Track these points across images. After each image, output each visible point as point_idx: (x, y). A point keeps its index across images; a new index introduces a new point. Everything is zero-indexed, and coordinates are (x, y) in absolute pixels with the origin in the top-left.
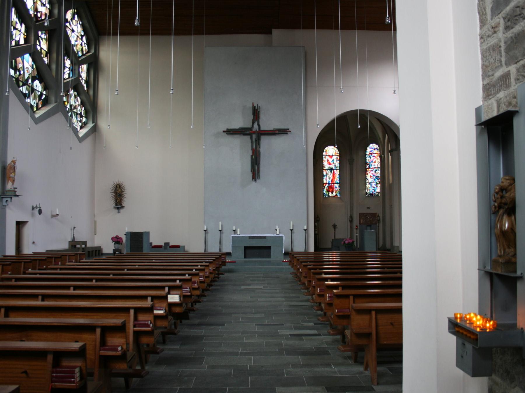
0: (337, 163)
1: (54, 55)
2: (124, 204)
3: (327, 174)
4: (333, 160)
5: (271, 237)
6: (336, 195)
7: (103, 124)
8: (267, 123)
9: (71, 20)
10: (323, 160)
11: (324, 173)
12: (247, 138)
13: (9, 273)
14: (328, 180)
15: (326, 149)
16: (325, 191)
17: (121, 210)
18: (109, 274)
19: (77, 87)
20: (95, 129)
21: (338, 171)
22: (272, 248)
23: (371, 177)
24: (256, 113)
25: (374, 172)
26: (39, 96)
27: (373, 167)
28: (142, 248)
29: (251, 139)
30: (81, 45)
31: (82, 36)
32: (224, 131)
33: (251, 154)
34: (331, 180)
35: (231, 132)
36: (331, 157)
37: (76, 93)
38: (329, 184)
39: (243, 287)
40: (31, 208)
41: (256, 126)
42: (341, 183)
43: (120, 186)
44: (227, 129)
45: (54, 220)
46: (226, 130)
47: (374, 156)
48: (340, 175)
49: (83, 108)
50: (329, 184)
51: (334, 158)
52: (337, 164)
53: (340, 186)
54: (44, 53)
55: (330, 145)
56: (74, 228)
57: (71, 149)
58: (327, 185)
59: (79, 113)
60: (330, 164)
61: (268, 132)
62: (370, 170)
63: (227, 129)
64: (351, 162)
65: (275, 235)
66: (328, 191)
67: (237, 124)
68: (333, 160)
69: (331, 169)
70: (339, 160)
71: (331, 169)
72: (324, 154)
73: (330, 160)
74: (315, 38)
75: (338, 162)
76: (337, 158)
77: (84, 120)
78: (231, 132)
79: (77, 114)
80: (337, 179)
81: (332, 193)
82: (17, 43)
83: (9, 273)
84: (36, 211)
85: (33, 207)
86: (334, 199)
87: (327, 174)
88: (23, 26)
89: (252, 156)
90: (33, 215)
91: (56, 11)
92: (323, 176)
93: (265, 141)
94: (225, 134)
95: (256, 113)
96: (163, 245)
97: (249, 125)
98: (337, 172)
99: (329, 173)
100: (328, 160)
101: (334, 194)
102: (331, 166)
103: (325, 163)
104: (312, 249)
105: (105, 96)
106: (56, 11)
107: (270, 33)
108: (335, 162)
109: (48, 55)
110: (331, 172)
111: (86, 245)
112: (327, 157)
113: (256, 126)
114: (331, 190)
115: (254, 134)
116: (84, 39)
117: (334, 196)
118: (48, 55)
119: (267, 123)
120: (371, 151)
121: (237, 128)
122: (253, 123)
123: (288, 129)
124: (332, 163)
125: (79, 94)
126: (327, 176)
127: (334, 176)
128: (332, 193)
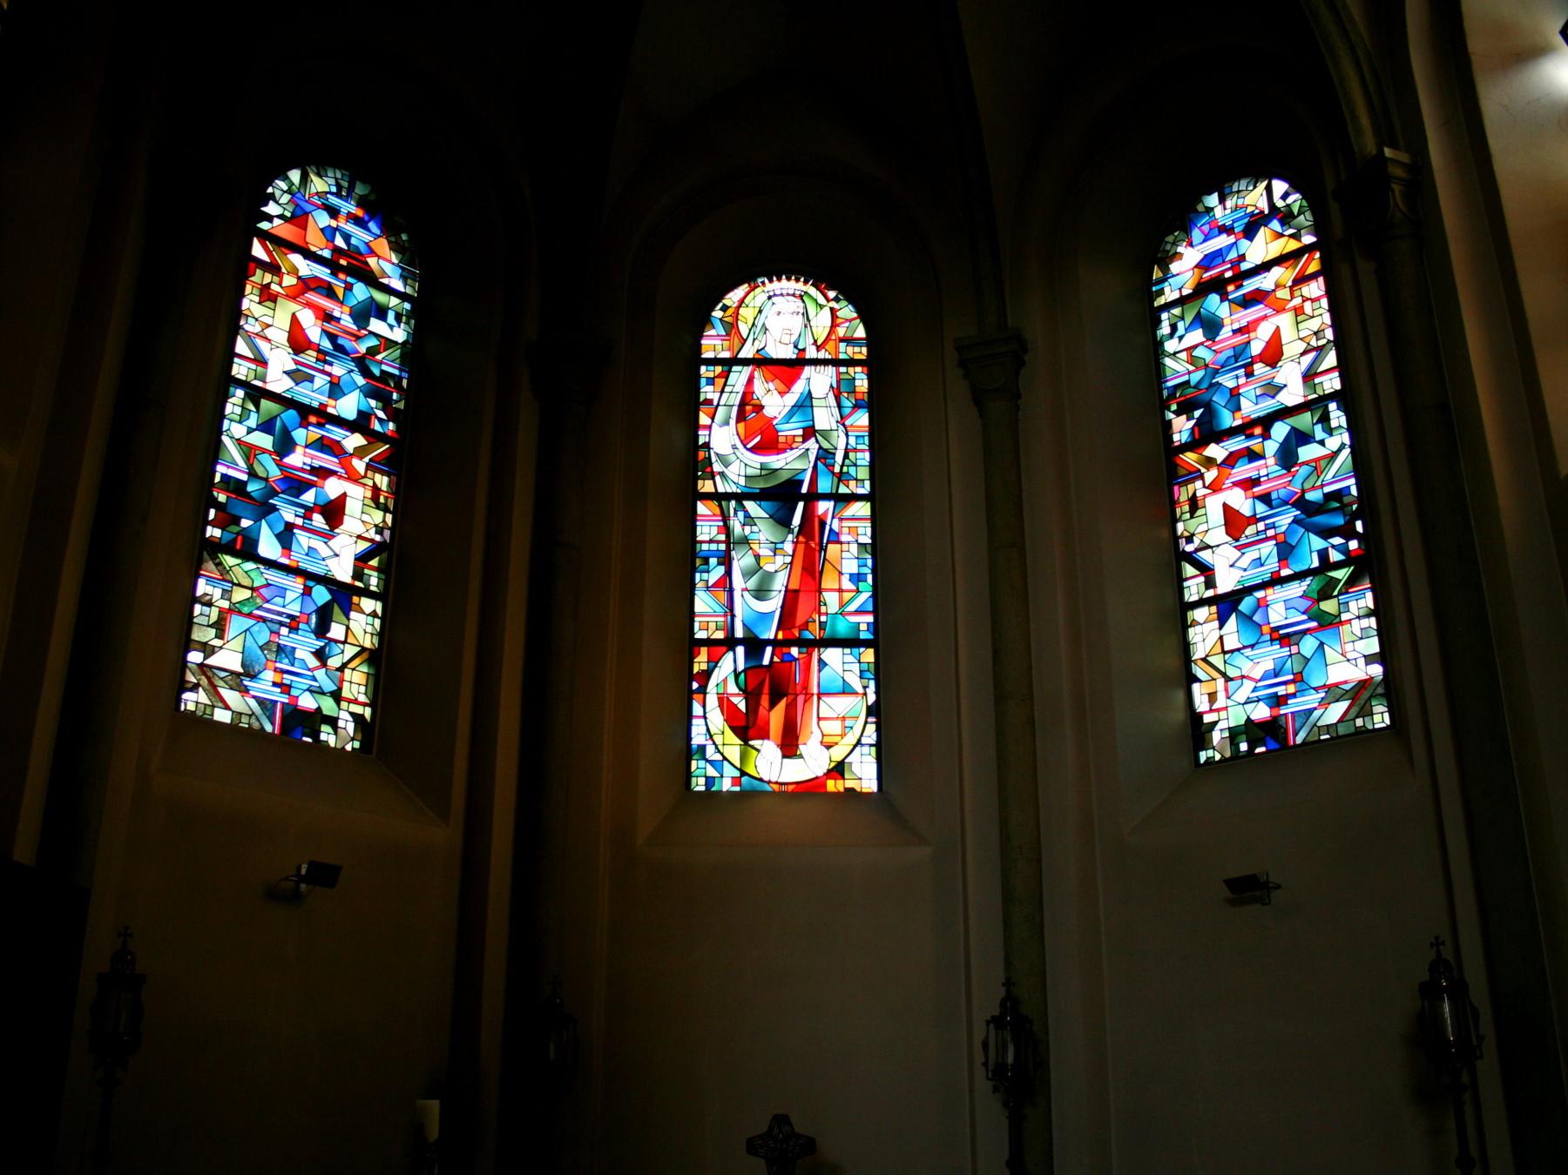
3: (732, 541)
4: (806, 403)
10: (693, 403)
14: (745, 605)
15: (732, 298)
16: (709, 723)
21: (863, 509)
27: (1251, 408)
34: (774, 604)
36: (787, 370)
42: (892, 644)
48: (876, 549)
51: (819, 381)
53: (880, 673)
55: (774, 273)
58: (730, 664)
64: (996, 372)
66: (747, 728)
69: (782, 496)
70: (874, 403)
71: (782, 496)
72: (713, 344)
73: (775, 403)
75: (862, 419)
80: (847, 597)
81: (789, 747)
87: (732, 541)
92: (688, 559)
99: (763, 532)
101: (811, 763)
103: (721, 437)
108: (824, 418)
110: (783, 521)
112: (739, 376)
114: (776, 717)
117: (811, 788)
124: (792, 429)
126: (742, 560)
127: (811, 567)
128: (789, 747)
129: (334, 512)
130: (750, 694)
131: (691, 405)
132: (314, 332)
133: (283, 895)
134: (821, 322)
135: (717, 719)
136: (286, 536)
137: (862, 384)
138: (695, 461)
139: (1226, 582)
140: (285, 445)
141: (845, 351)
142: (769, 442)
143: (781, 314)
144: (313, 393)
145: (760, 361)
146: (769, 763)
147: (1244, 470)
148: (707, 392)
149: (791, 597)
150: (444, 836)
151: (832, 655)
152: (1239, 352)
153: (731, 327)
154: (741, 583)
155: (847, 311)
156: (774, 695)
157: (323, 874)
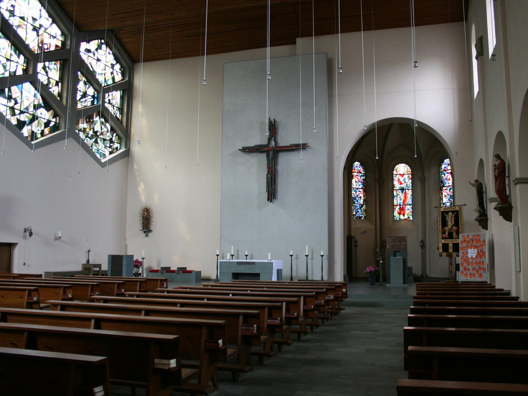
0: (409, 183)
1: (66, 84)
2: (152, 228)
3: (398, 195)
4: (405, 179)
5: (260, 263)
6: (409, 217)
7: (135, 148)
8: (285, 139)
9: (97, 50)
10: (393, 179)
11: (395, 193)
12: (264, 156)
13: (97, 293)
14: (399, 201)
15: (396, 167)
16: (396, 213)
17: (150, 234)
18: (203, 299)
19: (104, 114)
20: (127, 154)
21: (411, 191)
22: (261, 275)
23: (445, 196)
24: (273, 127)
25: (448, 191)
26: (45, 124)
27: (447, 185)
28: (122, 272)
29: (268, 156)
30: (112, 73)
31: (113, 66)
32: (239, 150)
33: (266, 173)
34: (402, 201)
35: (247, 150)
36: (402, 175)
37: (103, 120)
38: (400, 205)
39: (397, 316)
40: (23, 230)
41: (273, 143)
42: (413, 205)
43: (146, 209)
44: (243, 148)
45: (57, 241)
46: (241, 148)
47: (448, 173)
48: (412, 195)
49: (115, 134)
50: (400, 205)
51: (406, 176)
52: (408, 183)
53: (412, 208)
54: (53, 82)
55: (401, 163)
56: (89, 251)
57: (79, 173)
58: (398, 207)
59: (108, 138)
60: (401, 184)
61: (285, 149)
62: (444, 188)
63: (243, 148)
64: (423, 180)
65: (266, 261)
66: (400, 214)
67: (252, 143)
68: (405, 179)
69: (402, 189)
70: (412, 179)
71: (402, 189)
72: (395, 172)
73: (402, 179)
74: (338, 43)
75: (411, 181)
76: (409, 177)
77: (116, 145)
78: (247, 150)
79: (104, 140)
80: (409, 200)
81: (404, 215)
82: (13, 74)
83: (97, 293)
84: (28, 233)
85: (25, 229)
86: (406, 221)
87: (398, 195)
88: (22, 57)
89: (267, 175)
90: (25, 237)
91: (69, 42)
92: (393, 197)
93: (283, 159)
94: (240, 152)
95: (273, 127)
96: (160, 269)
97: (265, 142)
98: (409, 193)
99: (400, 194)
100: (399, 179)
101: (406, 217)
102: (402, 186)
103: (396, 183)
104: (339, 277)
105: (141, 122)
106: (69, 42)
107: (294, 43)
108: (407, 180)
109: (60, 84)
110: (403, 192)
111: (100, 268)
112: (398, 176)
113: (273, 143)
114: (402, 212)
115: (271, 151)
116: (118, 67)
117: (406, 219)
118: (60, 84)
119: (285, 139)
120: (445, 167)
121: (253, 145)
122: (269, 140)
123: (307, 144)
124: (403, 182)
125: (107, 121)
126: (398, 197)
127: (405, 197)
128: (404, 215)
129: (361, 197)
130: (400, 210)
131: (393, 180)
132: (357, 181)
133: (363, 233)
134: (406, 170)
135: (397, 213)
136: (357, 201)
137: (411, 176)
138: (393, 186)
139: (444, 202)
140: (356, 192)
141: (409, 173)
142: (401, 184)
143: (402, 169)
144: (357, 187)
145: (400, 174)
146: (402, 217)
147: (446, 191)
148: (394, 178)
149: (404, 201)
150: (373, 227)
151: (408, 206)
152: (447, 178)
153: (396, 170)
154: (398, 200)
155: (409, 168)
156: (402, 210)
157: (366, 232)
